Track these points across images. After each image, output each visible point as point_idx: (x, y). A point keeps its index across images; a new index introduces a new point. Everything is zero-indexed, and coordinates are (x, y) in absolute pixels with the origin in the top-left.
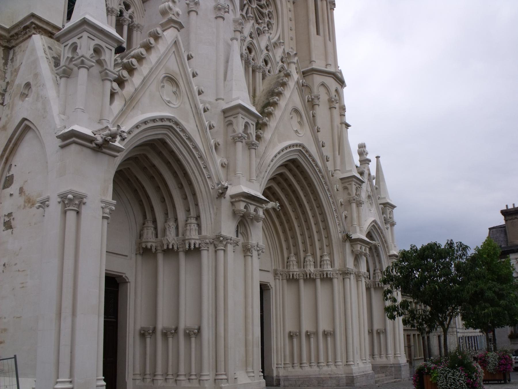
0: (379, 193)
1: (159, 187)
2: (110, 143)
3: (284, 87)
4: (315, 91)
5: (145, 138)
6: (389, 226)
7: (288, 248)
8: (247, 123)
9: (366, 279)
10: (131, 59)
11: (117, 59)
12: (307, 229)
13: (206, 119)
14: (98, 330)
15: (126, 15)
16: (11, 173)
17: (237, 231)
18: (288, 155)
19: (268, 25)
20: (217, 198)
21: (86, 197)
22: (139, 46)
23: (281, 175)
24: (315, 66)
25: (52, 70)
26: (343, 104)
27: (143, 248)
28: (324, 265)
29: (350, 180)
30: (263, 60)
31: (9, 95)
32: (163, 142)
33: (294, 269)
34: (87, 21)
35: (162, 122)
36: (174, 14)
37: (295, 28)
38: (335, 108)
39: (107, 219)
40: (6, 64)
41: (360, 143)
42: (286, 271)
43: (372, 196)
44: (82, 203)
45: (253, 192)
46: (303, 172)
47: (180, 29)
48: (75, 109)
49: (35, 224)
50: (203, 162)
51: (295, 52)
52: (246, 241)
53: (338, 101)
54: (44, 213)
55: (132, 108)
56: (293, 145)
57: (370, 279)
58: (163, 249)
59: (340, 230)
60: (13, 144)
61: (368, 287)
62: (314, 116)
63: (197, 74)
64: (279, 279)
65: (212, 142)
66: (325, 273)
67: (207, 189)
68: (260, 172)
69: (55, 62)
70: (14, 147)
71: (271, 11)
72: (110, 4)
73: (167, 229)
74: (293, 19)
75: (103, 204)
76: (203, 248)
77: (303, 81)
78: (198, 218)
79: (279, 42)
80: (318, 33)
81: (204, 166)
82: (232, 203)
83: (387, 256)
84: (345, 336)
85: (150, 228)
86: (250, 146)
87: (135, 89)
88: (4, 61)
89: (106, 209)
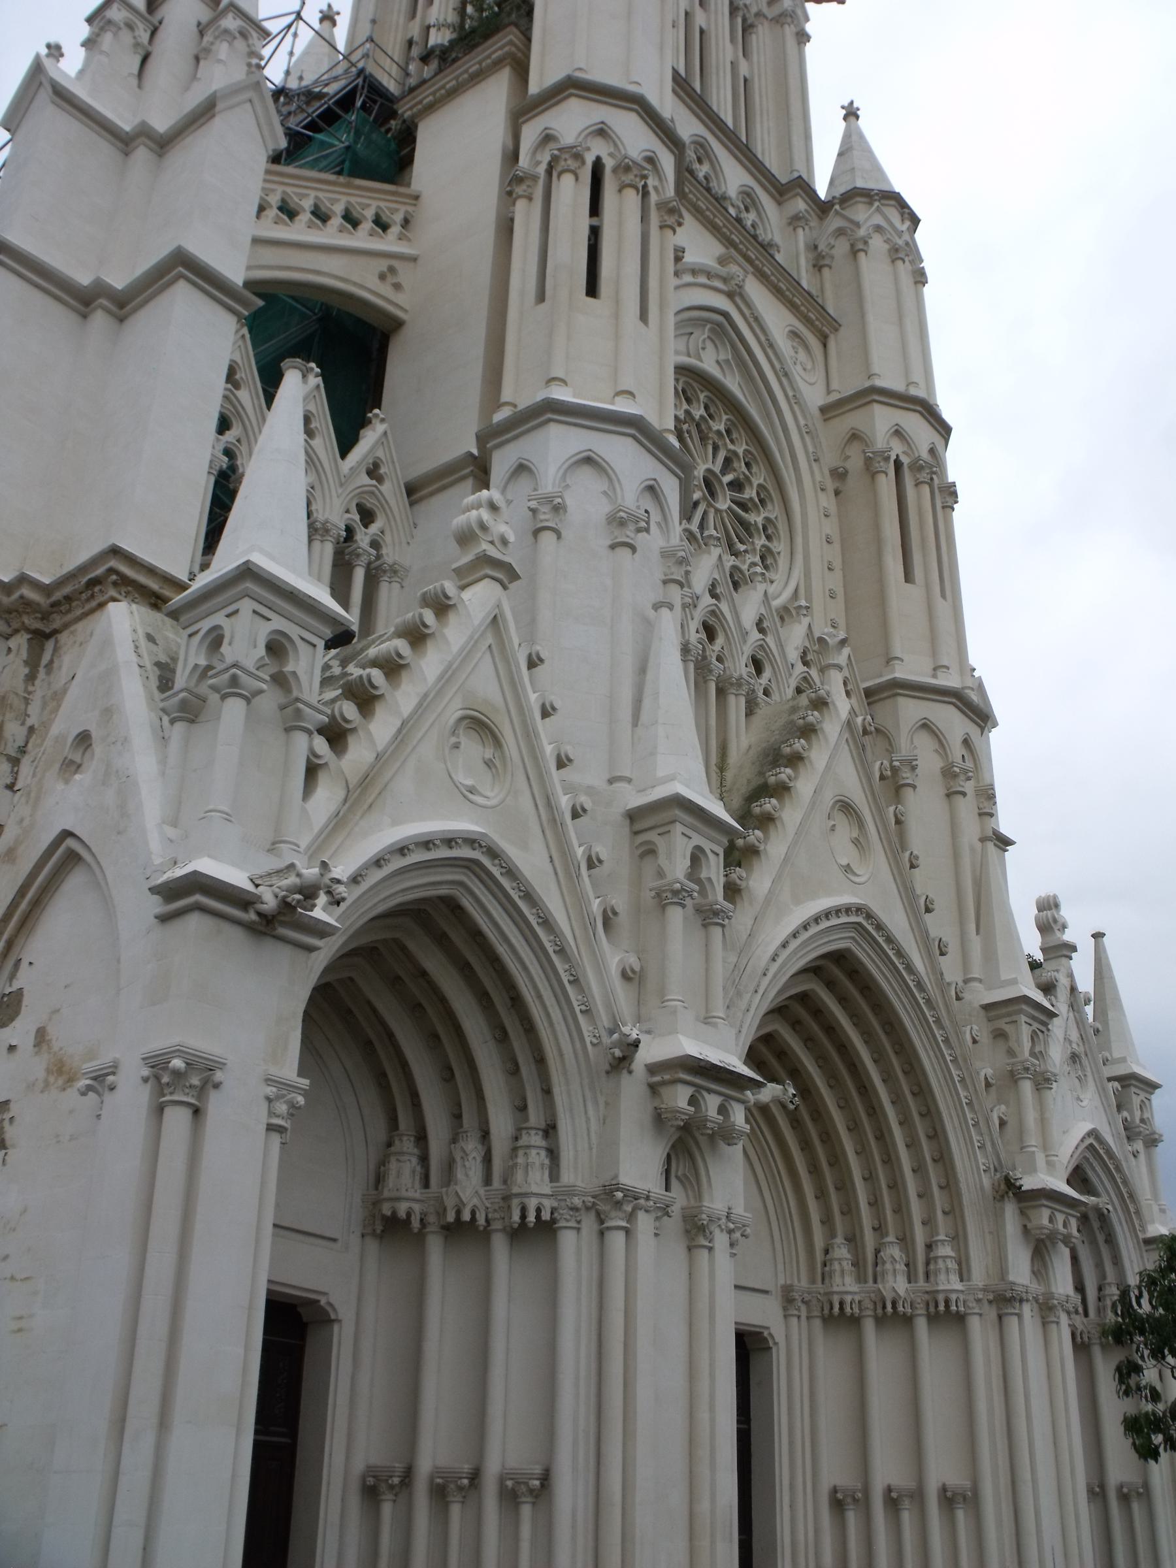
0: (1106, 1045)
1: (435, 1037)
2: (299, 910)
3: (808, 739)
4: (904, 747)
5: (401, 894)
6: (1139, 1145)
7: (827, 1221)
8: (698, 848)
9: (1073, 1316)
10: (368, 670)
11: (331, 663)
12: (884, 1162)
13: (578, 838)
14: (234, 1476)
15: (362, 540)
16: (16, 985)
17: (667, 1172)
18: (822, 938)
19: (763, 558)
20: (608, 1073)
21: (222, 1065)
22: (392, 629)
23: (803, 998)
24: (900, 672)
25: (151, 699)
26: (988, 782)
27: (385, 1219)
28: (937, 1272)
29: (1011, 1009)
30: (748, 659)
31: (33, 761)
32: (452, 906)
33: (846, 1285)
34: (255, 569)
35: (451, 848)
36: (492, 542)
37: (843, 562)
38: (964, 794)
39: (281, 1133)
40: (31, 678)
41: (1043, 895)
42: (822, 1291)
43: (1083, 1056)
44: (209, 1084)
45: (715, 1056)
46: (868, 987)
47: (510, 582)
48: (206, 812)
49: (70, 1140)
50: (567, 967)
51: (842, 635)
52: (693, 1203)
53: (970, 774)
54: (101, 1109)
55: (366, 807)
56: (838, 911)
57: (1086, 1314)
58: (442, 1223)
59: (984, 1164)
60: (29, 903)
61: (1083, 1343)
62: (898, 822)
63: (554, 709)
64: (799, 1317)
65: (596, 906)
66: (941, 1298)
67: (578, 1045)
68: (739, 994)
69: (161, 678)
70: (31, 911)
71: (772, 517)
72: (321, 511)
73: (458, 1159)
74: (836, 538)
75: (270, 1088)
76: (562, 1224)
77: (864, 719)
78: (550, 1130)
79: (796, 604)
80: (908, 577)
81: (572, 978)
82: (654, 1089)
83: (1138, 1242)
84: (1011, 1507)
85: (406, 1158)
86: (709, 917)
87: (375, 756)
88: (26, 670)
89: (278, 1104)
